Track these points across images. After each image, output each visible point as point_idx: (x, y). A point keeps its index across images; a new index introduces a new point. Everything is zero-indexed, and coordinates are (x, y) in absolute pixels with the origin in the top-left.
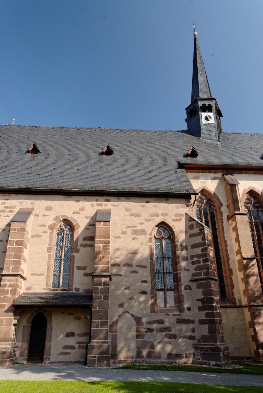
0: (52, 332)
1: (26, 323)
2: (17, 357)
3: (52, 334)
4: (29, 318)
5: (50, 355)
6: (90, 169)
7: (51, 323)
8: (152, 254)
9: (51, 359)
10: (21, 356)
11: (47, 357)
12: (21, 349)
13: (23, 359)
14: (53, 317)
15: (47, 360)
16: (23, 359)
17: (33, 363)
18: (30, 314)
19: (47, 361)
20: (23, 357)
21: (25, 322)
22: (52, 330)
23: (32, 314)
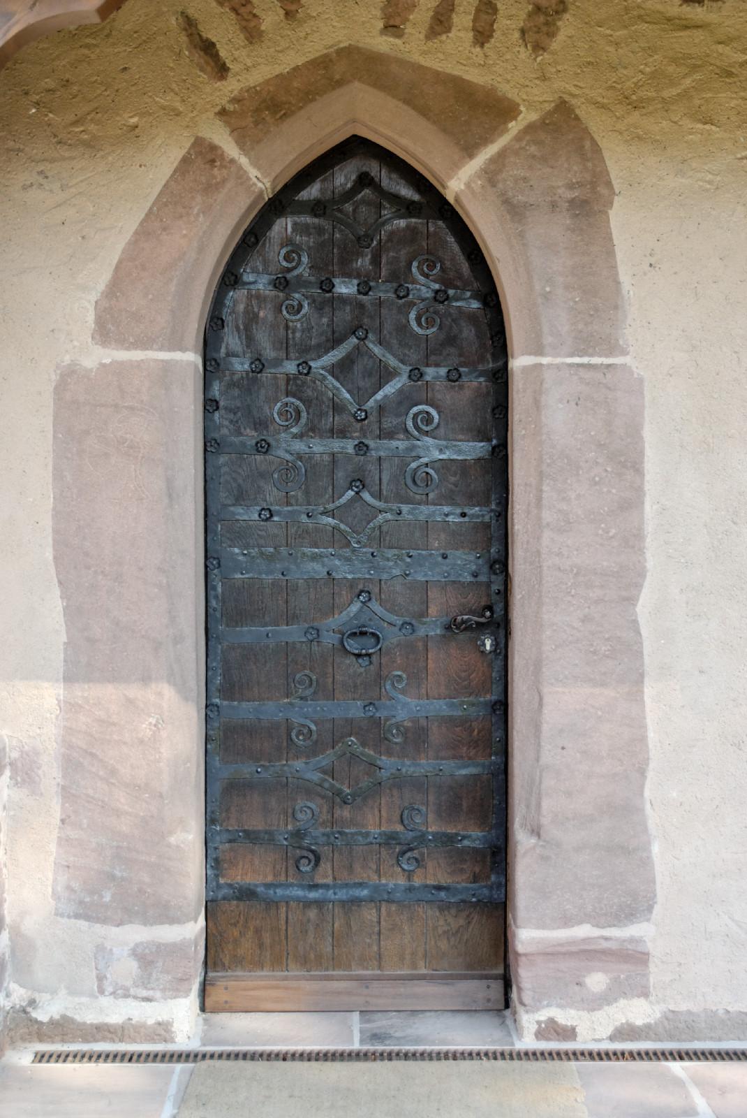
0: (632, 503)
1: (105, 331)
2: (29, 926)
3: (633, 540)
4: (144, 232)
5: (636, 905)
6: (245, 468)
7: (612, 347)
8: (385, 1038)
9: (656, 974)
10: (88, 911)
11: (583, 931)
12: (67, 793)
13: (147, 958)
14: (621, 219)
15: (597, 981)
16: (147, 958)
17: (515, 855)
18: (162, 160)
19: (596, 1003)
20: (137, 934)
21: (83, 309)
22: (627, 462)
23: (205, 154)
